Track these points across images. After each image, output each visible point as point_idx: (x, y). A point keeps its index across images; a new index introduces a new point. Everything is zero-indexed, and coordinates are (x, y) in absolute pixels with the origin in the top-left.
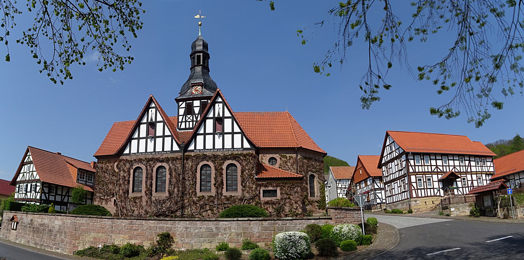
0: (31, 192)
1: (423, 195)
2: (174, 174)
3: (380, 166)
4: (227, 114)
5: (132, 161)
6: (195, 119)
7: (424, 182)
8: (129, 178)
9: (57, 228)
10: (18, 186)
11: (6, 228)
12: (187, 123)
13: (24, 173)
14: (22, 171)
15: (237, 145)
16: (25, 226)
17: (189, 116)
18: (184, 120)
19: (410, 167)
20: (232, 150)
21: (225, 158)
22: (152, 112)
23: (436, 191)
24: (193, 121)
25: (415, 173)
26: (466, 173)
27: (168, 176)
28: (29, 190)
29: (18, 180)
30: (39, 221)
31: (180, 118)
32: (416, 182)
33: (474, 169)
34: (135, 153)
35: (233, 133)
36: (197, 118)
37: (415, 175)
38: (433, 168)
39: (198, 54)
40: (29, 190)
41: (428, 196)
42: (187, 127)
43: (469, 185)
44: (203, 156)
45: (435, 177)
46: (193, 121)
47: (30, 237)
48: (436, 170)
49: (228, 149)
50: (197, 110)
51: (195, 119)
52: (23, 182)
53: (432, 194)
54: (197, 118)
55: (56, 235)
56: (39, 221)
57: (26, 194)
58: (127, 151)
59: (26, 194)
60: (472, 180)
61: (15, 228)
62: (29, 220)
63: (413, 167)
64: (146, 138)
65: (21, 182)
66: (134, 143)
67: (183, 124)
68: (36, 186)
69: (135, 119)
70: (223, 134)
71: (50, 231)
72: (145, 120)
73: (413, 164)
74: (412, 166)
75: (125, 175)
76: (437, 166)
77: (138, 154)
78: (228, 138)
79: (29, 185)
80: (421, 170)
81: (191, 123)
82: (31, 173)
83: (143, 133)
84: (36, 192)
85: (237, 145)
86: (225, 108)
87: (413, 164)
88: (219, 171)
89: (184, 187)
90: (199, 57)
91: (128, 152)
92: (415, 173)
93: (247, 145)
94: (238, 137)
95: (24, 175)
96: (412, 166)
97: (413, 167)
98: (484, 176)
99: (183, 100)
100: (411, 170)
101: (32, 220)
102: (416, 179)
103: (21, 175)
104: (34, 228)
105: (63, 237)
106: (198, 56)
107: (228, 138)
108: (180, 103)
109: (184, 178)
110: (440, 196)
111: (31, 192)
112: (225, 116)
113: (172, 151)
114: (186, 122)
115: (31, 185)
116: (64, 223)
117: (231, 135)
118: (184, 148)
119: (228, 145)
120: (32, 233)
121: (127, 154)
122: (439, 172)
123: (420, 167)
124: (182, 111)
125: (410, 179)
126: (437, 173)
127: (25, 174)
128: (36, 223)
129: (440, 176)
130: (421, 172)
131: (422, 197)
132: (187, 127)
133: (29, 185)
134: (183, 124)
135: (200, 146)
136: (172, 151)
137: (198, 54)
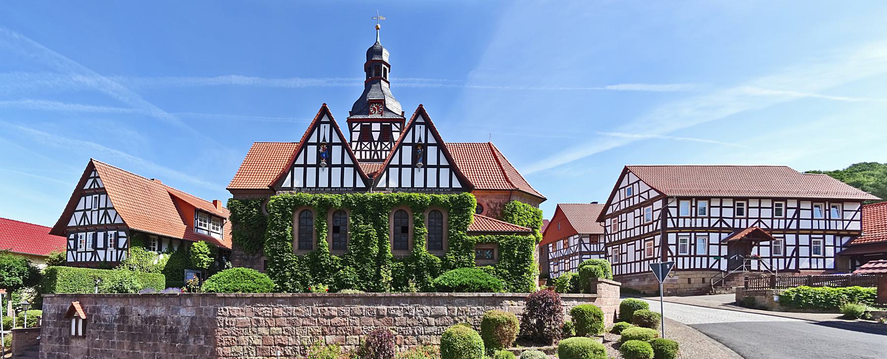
0: (105, 248)
1: (686, 267)
3: (602, 218)
4: (431, 140)
6: (373, 148)
7: (691, 244)
9: (185, 324)
10: (72, 236)
11: (55, 337)
12: (363, 153)
13: (85, 210)
14: (81, 206)
16: (107, 327)
17: (366, 143)
18: (359, 148)
19: (669, 220)
22: (325, 130)
23: (712, 261)
24: (370, 150)
25: (677, 229)
26: (786, 231)
28: (100, 244)
29: (72, 223)
30: (142, 311)
31: (354, 144)
32: (677, 245)
33: (805, 225)
36: (376, 147)
37: (677, 233)
38: (713, 221)
40: (100, 244)
41: (695, 269)
42: (363, 157)
43: (789, 254)
45: (714, 237)
46: (370, 150)
47: (125, 350)
48: (718, 225)
50: (376, 136)
51: (373, 148)
52: (86, 229)
53: (704, 266)
54: (376, 147)
55: (185, 339)
56: (142, 311)
57: (94, 253)
58: (287, 183)
59: (94, 253)
60: (797, 246)
61: (80, 333)
62: (116, 312)
63: (675, 220)
64: (318, 166)
65: (78, 229)
66: (299, 171)
67: (358, 153)
68: (117, 237)
69: (299, 138)
71: (171, 331)
72: (313, 139)
73: (674, 214)
74: (672, 218)
76: (721, 219)
79: (101, 235)
80: (687, 225)
81: (368, 153)
82: (102, 212)
83: (312, 159)
84: (118, 249)
87: (674, 214)
92: (677, 229)
95: (85, 215)
96: (672, 218)
97: (675, 220)
98: (829, 239)
99: (358, 121)
100: (670, 224)
101: (122, 311)
102: (677, 240)
103: (78, 215)
104: (130, 328)
105: (202, 342)
108: (354, 125)
110: (719, 269)
111: (105, 248)
114: (361, 150)
115: (106, 236)
116: (200, 311)
120: (126, 342)
122: (725, 228)
123: (688, 220)
124: (356, 136)
125: (664, 240)
126: (720, 230)
127: (88, 213)
128: (134, 317)
129: (724, 236)
130: (688, 228)
131: (683, 270)
132: (363, 157)
133: (101, 235)
134: (358, 153)
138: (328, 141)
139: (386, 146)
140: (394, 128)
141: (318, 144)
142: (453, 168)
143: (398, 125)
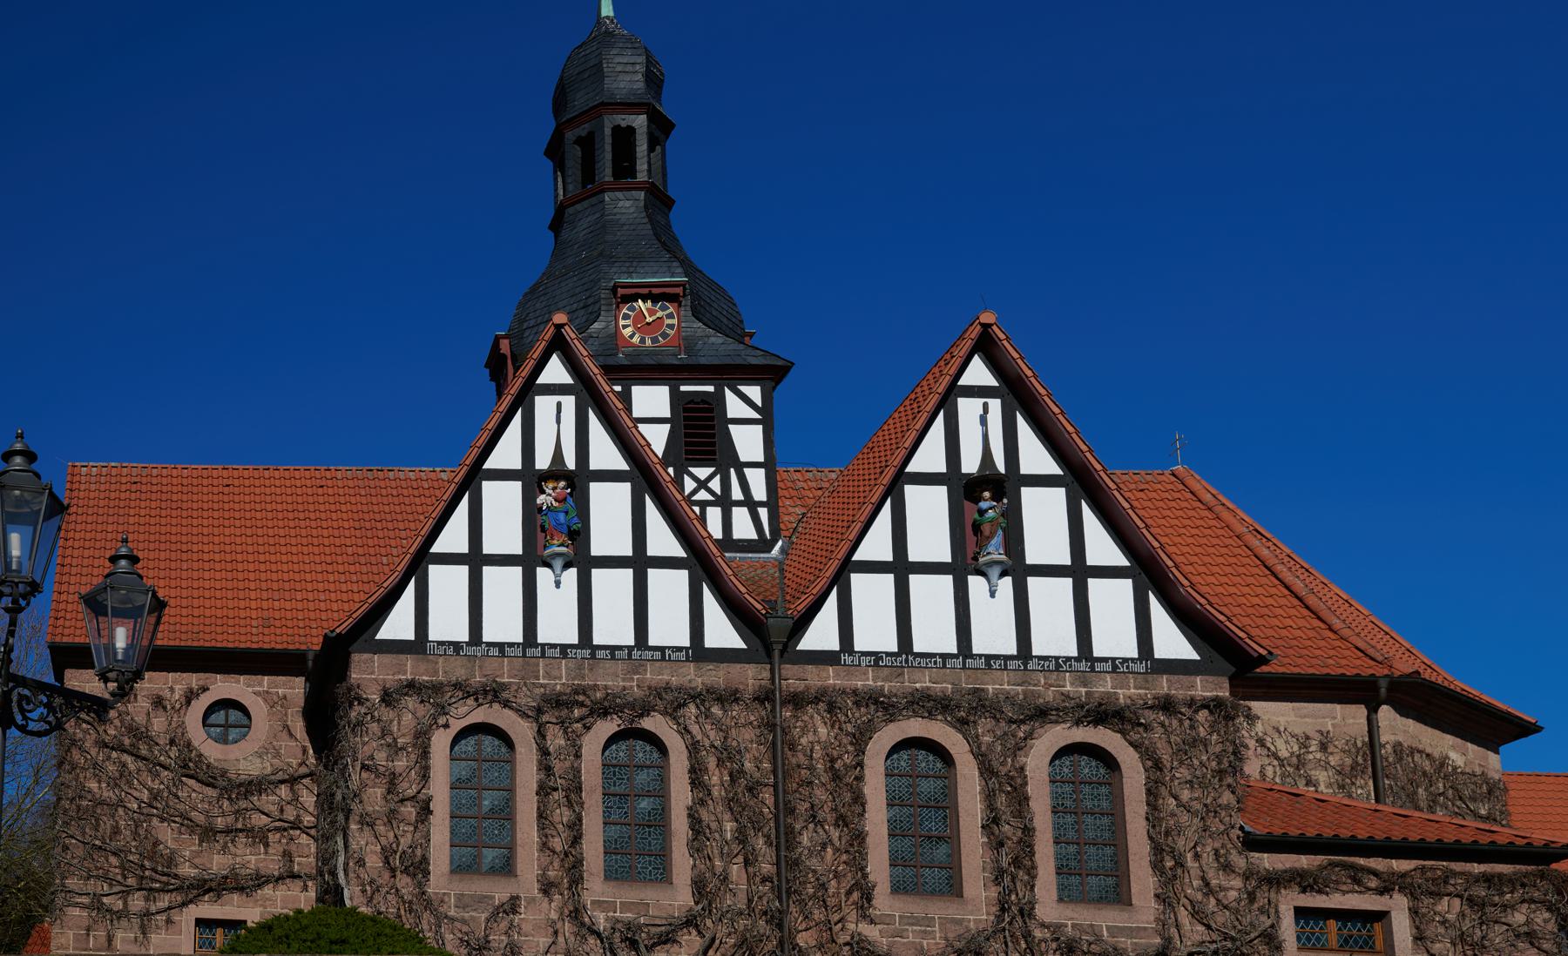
2: (716, 778)
4: (1035, 457)
5: (437, 688)
8: (425, 777)
15: (669, 628)
20: (1083, 666)
21: (886, 707)
27: (681, 794)
34: (456, 645)
35: (640, 562)
39: (624, 120)
44: (470, 678)
58: (398, 624)
70: (584, 562)
75: (401, 764)
77: (478, 651)
78: (612, 588)
85: (669, 628)
86: (1022, 425)
88: (1006, 790)
89: (788, 863)
90: (624, 137)
91: (410, 635)
93: (1171, 642)
94: (669, 588)
106: (617, 129)
107: (612, 588)
109: (785, 809)
112: (593, 466)
113: (698, 651)
117: (463, 570)
118: (770, 632)
119: (613, 627)
121: (396, 647)
135: (448, 623)
136: (698, 651)
137: (624, 120)
138: (570, 463)
139: (702, 484)
140: (735, 407)
141: (530, 478)
142: (1149, 574)
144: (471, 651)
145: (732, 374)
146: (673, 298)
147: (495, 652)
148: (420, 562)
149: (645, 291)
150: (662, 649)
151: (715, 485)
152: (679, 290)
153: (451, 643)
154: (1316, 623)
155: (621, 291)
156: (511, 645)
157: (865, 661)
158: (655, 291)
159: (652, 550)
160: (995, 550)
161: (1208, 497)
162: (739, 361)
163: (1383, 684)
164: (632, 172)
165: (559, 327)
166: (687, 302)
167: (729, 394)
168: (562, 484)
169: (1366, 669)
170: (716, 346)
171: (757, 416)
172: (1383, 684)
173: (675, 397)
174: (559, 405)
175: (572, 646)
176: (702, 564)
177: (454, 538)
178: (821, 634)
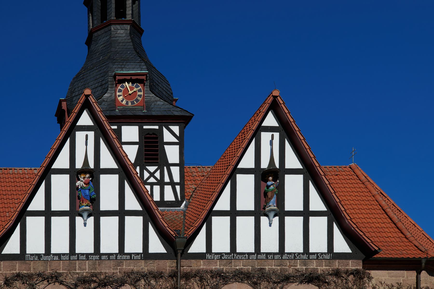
4: (292, 161)
35: (122, 213)
49: (295, 256)
66: (35, 226)
77: (49, 258)
91: (18, 251)
93: (341, 245)
94: (134, 225)
121: (12, 257)
139: (152, 175)
140: (167, 137)
141: (74, 173)
143: (176, 129)
144: (46, 258)
145: (166, 120)
146: (141, 82)
147: (56, 258)
148: (23, 214)
149: (129, 78)
150: (130, 254)
151: (157, 175)
152: (144, 77)
153: (36, 255)
154: (401, 235)
155: (118, 78)
156: (64, 254)
157: (216, 257)
158: (134, 78)
159: (128, 207)
160: (272, 205)
161: (363, 178)
162: (170, 114)
163: (424, 261)
164: (124, 15)
165: (87, 96)
166: (147, 83)
167: (165, 130)
168: (88, 176)
169: (417, 254)
170: (160, 106)
171: (176, 140)
172: (424, 261)
173: (141, 131)
174: (87, 136)
175: (91, 254)
176: (148, 213)
177: (38, 203)
178: (198, 246)
